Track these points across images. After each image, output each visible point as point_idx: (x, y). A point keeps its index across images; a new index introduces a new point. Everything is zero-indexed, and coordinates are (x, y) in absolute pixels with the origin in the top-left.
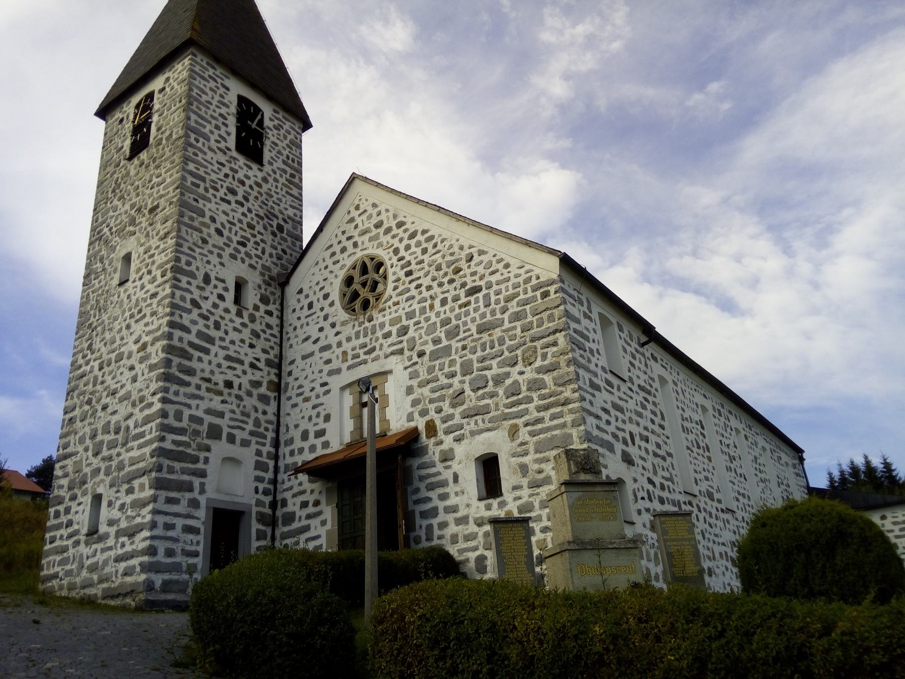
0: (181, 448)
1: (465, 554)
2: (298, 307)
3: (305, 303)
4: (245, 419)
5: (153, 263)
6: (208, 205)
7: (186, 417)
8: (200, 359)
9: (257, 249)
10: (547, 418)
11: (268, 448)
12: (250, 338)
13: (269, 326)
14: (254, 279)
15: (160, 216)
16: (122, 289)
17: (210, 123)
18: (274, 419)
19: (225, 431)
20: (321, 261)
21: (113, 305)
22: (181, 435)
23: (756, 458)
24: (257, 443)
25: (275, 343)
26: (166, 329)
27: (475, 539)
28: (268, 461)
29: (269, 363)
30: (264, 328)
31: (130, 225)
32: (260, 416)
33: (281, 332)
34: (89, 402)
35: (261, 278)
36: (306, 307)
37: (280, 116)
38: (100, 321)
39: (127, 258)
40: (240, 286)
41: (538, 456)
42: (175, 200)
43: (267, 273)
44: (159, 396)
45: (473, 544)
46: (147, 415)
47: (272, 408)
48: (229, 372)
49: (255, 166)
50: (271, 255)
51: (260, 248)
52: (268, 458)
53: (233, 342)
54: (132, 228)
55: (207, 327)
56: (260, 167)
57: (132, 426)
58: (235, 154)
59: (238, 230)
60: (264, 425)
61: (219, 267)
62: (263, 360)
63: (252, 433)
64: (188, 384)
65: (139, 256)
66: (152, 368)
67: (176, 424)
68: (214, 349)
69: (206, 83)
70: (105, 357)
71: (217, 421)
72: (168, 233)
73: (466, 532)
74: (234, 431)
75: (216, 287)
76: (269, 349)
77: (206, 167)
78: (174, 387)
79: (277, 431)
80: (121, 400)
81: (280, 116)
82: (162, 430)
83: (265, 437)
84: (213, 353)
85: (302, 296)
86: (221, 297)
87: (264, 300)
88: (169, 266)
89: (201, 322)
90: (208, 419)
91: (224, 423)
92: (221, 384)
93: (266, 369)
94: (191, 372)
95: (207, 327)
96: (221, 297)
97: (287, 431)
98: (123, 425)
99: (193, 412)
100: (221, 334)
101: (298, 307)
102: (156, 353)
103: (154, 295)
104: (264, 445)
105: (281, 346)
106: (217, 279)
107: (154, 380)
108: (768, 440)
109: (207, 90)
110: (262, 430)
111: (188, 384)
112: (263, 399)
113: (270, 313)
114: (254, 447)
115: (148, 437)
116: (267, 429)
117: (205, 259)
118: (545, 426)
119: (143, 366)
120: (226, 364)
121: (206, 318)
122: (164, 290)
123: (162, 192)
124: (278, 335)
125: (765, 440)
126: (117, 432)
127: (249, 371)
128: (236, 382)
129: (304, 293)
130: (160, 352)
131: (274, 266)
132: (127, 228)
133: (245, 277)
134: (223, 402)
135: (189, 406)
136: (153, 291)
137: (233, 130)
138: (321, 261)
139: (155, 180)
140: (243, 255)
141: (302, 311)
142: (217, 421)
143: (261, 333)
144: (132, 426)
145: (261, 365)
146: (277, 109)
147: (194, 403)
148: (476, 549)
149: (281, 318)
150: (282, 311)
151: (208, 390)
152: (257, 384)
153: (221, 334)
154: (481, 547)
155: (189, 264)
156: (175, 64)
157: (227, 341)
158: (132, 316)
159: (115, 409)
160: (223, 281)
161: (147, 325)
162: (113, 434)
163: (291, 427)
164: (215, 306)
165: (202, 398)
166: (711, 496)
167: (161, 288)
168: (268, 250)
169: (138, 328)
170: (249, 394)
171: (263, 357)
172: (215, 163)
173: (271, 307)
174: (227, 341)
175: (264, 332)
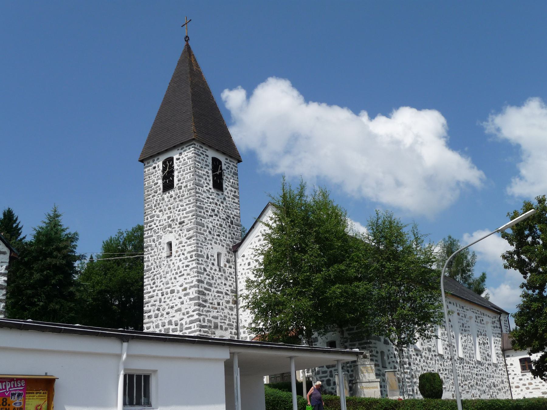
1: (322, 378)
2: (243, 264)
3: (247, 262)
4: (225, 318)
5: (185, 250)
6: (205, 220)
8: (208, 294)
10: (355, 329)
11: (234, 331)
13: (230, 274)
14: (224, 251)
20: (253, 243)
21: (164, 266)
22: (205, 328)
23: (463, 324)
26: (196, 283)
29: (232, 292)
30: (229, 275)
31: (168, 227)
33: (236, 275)
34: (158, 310)
36: (247, 264)
37: (228, 161)
38: (158, 272)
39: (170, 244)
40: (219, 255)
41: (351, 343)
42: (193, 221)
44: (197, 312)
45: (326, 375)
47: (234, 312)
49: (220, 193)
50: (229, 238)
51: (225, 236)
52: (234, 335)
53: (218, 284)
54: (170, 229)
55: (209, 279)
56: (222, 193)
57: (184, 323)
59: (216, 229)
60: (232, 320)
62: (229, 290)
64: (205, 306)
65: (176, 245)
66: (191, 299)
68: (212, 289)
70: (164, 291)
71: (216, 321)
72: (191, 237)
73: (323, 370)
76: (231, 285)
77: (203, 202)
79: (237, 322)
80: (176, 311)
81: (228, 161)
82: (200, 327)
83: (233, 326)
85: (244, 259)
86: (213, 264)
87: (228, 261)
88: (194, 253)
89: (208, 277)
90: (213, 320)
93: (231, 294)
96: (213, 264)
97: (241, 322)
98: (179, 322)
100: (214, 281)
101: (243, 264)
102: (193, 293)
103: (187, 266)
104: (232, 329)
105: (236, 282)
106: (211, 256)
107: (193, 305)
108: (475, 311)
110: (231, 323)
111: (205, 306)
112: (231, 309)
113: (230, 267)
114: (229, 330)
115: (193, 329)
116: (233, 322)
119: (186, 298)
120: (217, 295)
121: (209, 275)
122: (192, 264)
123: (185, 215)
124: (234, 277)
125: (474, 312)
126: (176, 325)
127: (225, 296)
129: (245, 257)
130: (194, 293)
131: (231, 243)
134: (217, 312)
136: (186, 264)
137: (211, 178)
138: (253, 243)
139: (180, 207)
140: (219, 241)
144: (184, 323)
145: (229, 293)
146: (227, 158)
147: (208, 314)
148: (326, 377)
149: (235, 269)
150: (235, 265)
151: (212, 308)
152: (228, 302)
153: (214, 281)
154: (328, 376)
155: (201, 252)
156: (185, 147)
157: (217, 284)
158: (177, 273)
160: (213, 256)
161: (185, 279)
162: (174, 326)
163: (243, 320)
164: (211, 269)
166: (429, 350)
167: (191, 263)
168: (228, 235)
169: (181, 280)
171: (229, 289)
172: (206, 198)
173: (231, 264)
174: (217, 284)
175: (229, 276)
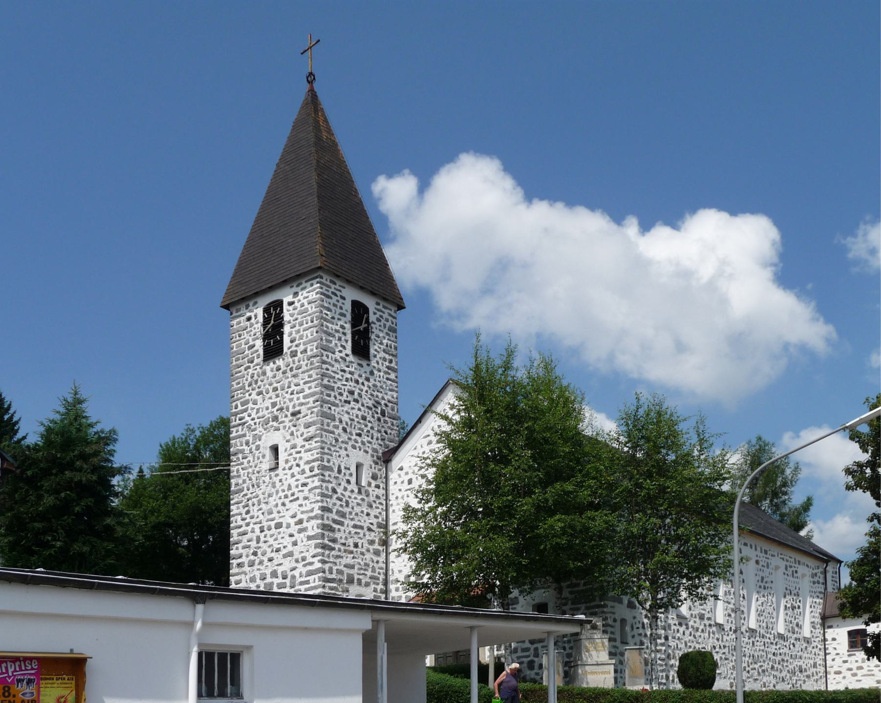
0: (333, 592)
2: (399, 481)
3: (406, 478)
6: (337, 409)
7: (334, 572)
8: (339, 530)
9: (368, 436)
10: (582, 584)
11: (380, 587)
12: (367, 509)
14: (367, 461)
15: (302, 421)
16: (273, 474)
17: (334, 336)
18: (384, 566)
19: (356, 577)
22: (333, 583)
24: (374, 583)
25: (382, 509)
27: (528, 651)
28: (381, 595)
29: (379, 526)
32: (375, 565)
35: (372, 459)
36: (406, 482)
37: (380, 307)
39: (275, 449)
40: (359, 466)
41: (573, 606)
43: (375, 454)
46: (310, 570)
47: (382, 558)
48: (356, 536)
52: (381, 593)
53: (357, 514)
54: (275, 424)
58: (351, 358)
59: (356, 424)
60: (378, 570)
61: (346, 458)
63: (371, 578)
64: (333, 549)
65: (286, 450)
66: (309, 538)
67: (330, 577)
68: (346, 522)
69: (329, 300)
70: (265, 524)
71: (351, 572)
74: (361, 577)
75: (345, 474)
76: (378, 515)
77: (334, 378)
78: (327, 552)
79: (386, 574)
83: (378, 579)
84: (346, 524)
85: (402, 473)
86: (348, 482)
87: (374, 477)
89: (339, 503)
90: (346, 571)
91: (354, 572)
92: (352, 545)
93: (377, 530)
94: (334, 541)
95: (341, 506)
96: (348, 482)
97: (393, 573)
98: (290, 574)
99: (338, 567)
100: (349, 509)
101: (399, 481)
102: (313, 528)
104: (378, 584)
106: (346, 468)
109: (331, 307)
110: (376, 574)
111: (333, 549)
112: (377, 553)
113: (378, 487)
114: (373, 586)
116: (379, 574)
117: (337, 454)
118: (579, 589)
120: (353, 531)
121: (341, 500)
122: (313, 482)
126: (285, 577)
127: (367, 533)
128: (360, 542)
130: (315, 528)
132: (271, 423)
133: (362, 462)
135: (335, 563)
136: (303, 481)
137: (349, 337)
138: (419, 447)
139: (293, 387)
140: (360, 444)
141: (403, 484)
142: (351, 572)
143: (373, 503)
145: (374, 528)
147: (338, 561)
149: (386, 489)
150: (387, 484)
151: (345, 551)
152: (372, 542)
153: (349, 509)
154: (532, 656)
157: (353, 514)
158: (286, 497)
159: (281, 562)
160: (349, 469)
162: (281, 579)
164: (345, 489)
165: (342, 557)
167: (311, 479)
168: (376, 435)
169: (294, 507)
170: (368, 551)
171: (375, 521)
172: (339, 372)
173: (379, 482)
174: (353, 514)
175: (375, 502)
